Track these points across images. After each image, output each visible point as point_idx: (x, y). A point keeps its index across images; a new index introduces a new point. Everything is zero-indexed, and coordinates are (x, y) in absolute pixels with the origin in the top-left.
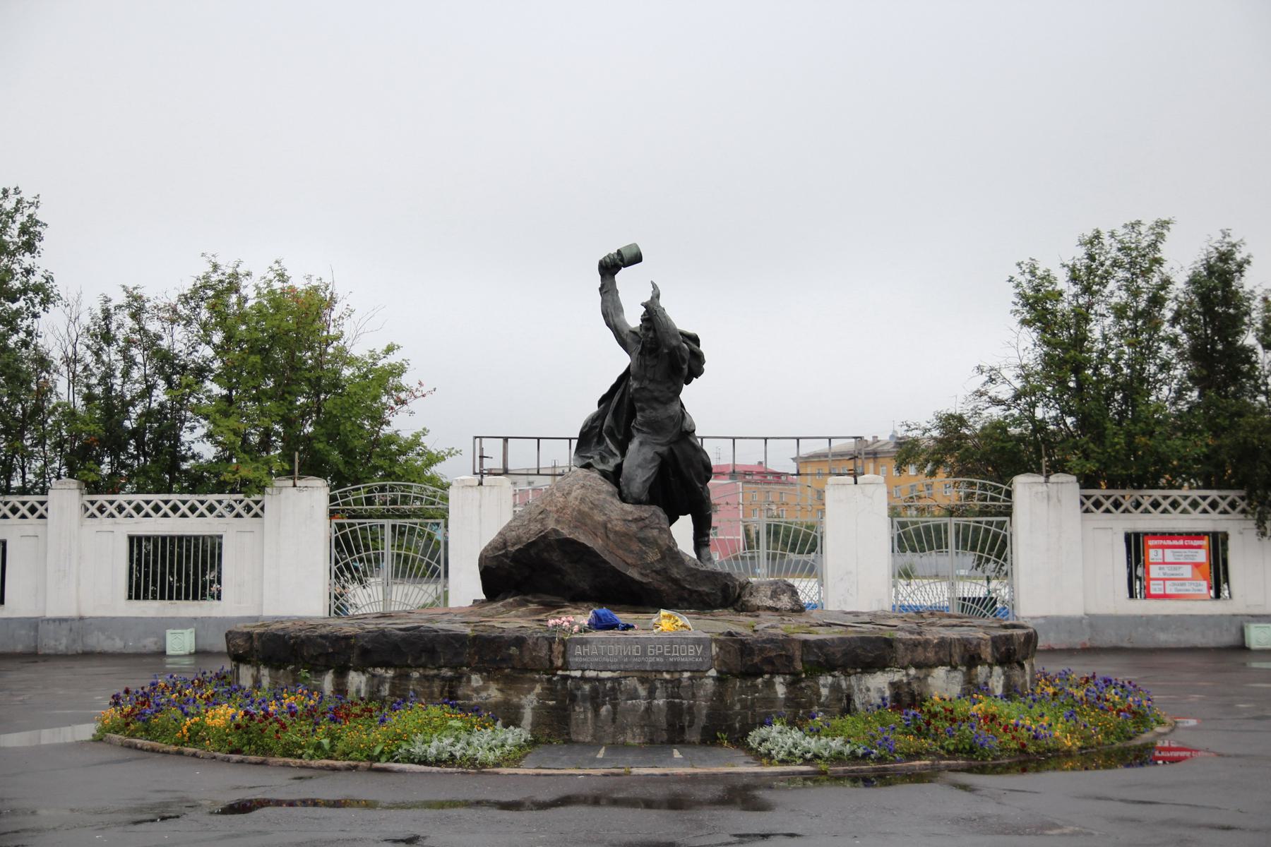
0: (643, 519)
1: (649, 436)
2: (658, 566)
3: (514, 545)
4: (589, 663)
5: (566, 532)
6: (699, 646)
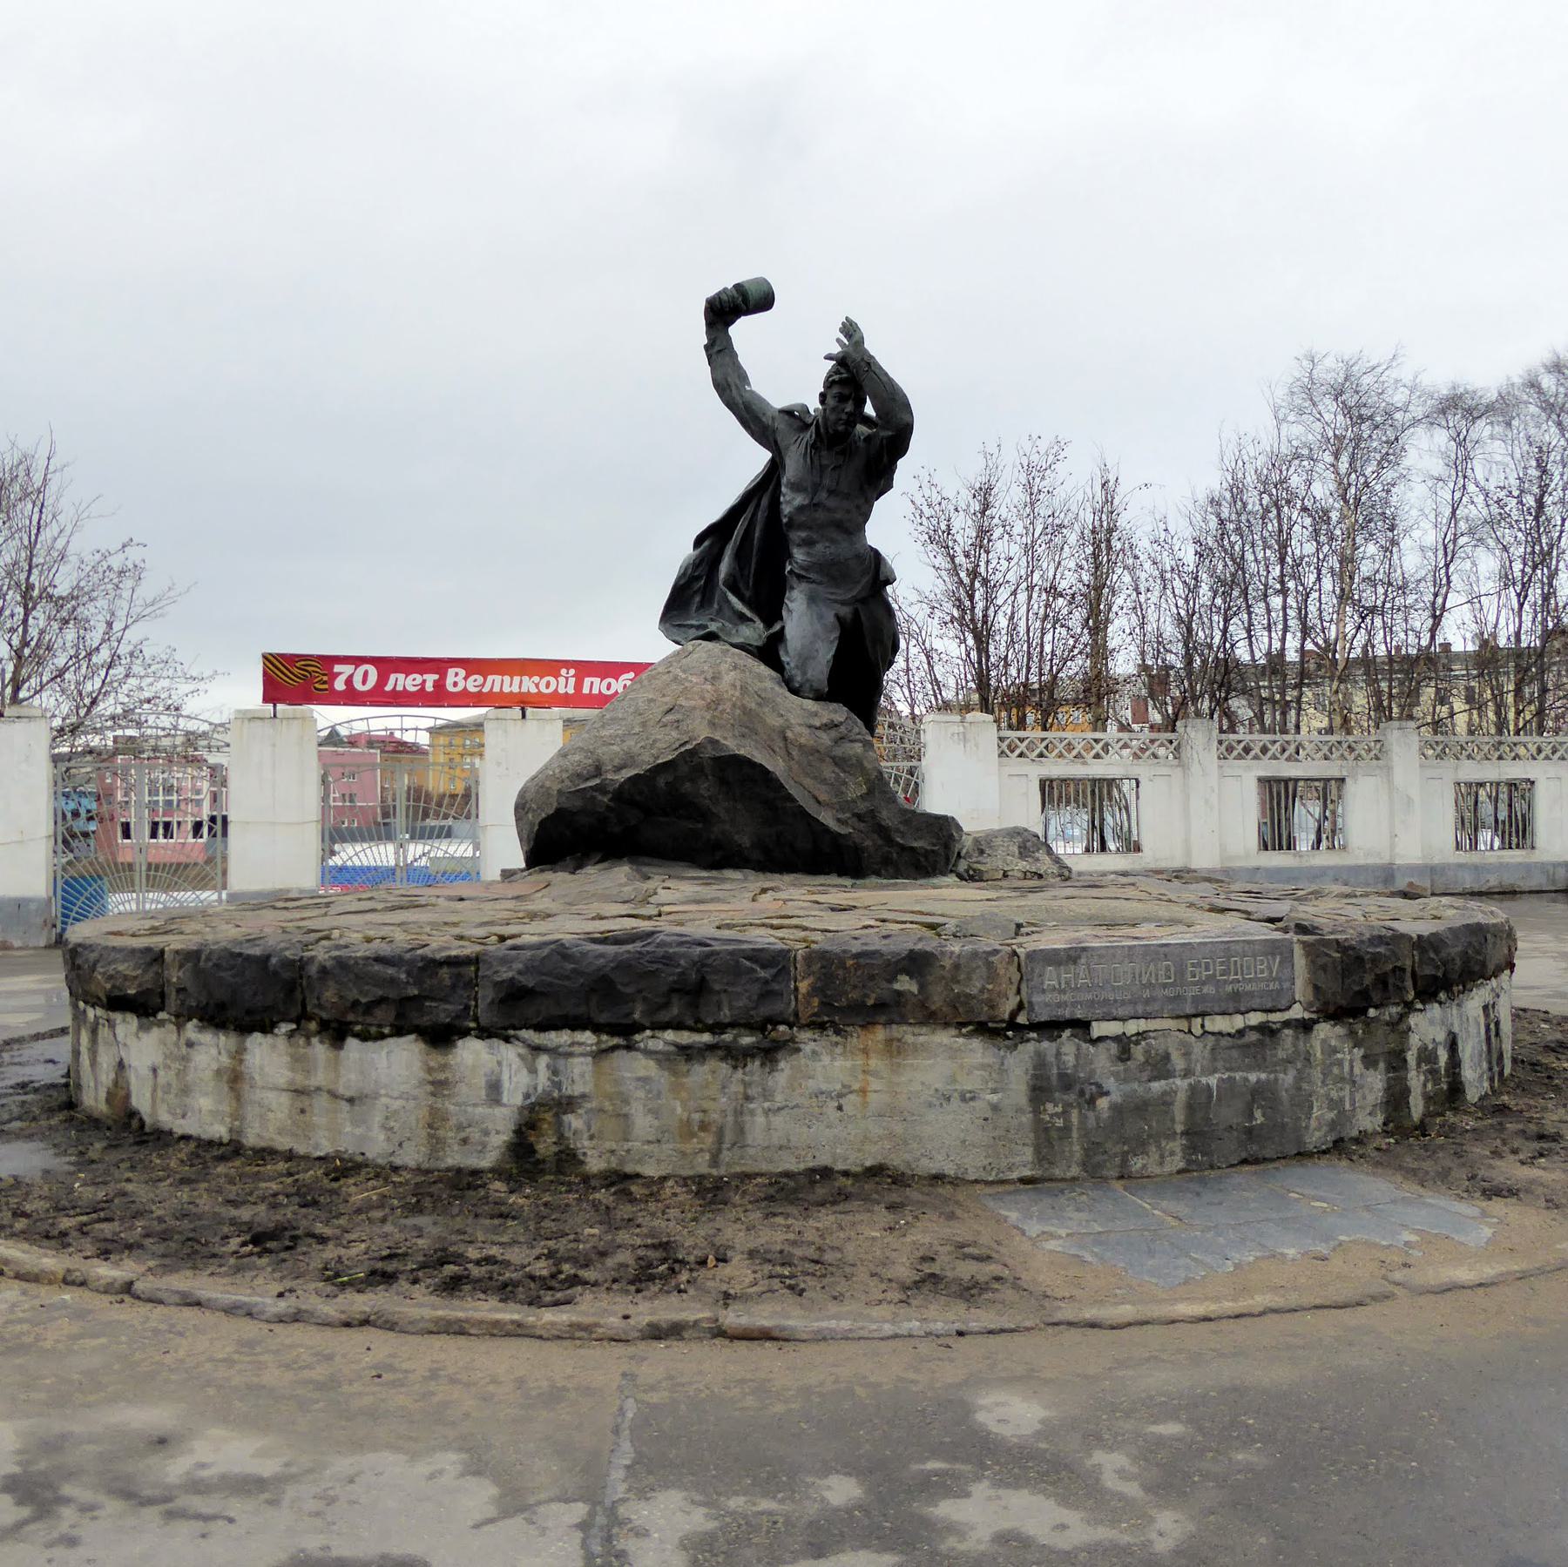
0: (836, 726)
1: (820, 588)
2: (862, 807)
3: (618, 769)
4: (1074, 1004)
5: (734, 745)
6: (1273, 954)
